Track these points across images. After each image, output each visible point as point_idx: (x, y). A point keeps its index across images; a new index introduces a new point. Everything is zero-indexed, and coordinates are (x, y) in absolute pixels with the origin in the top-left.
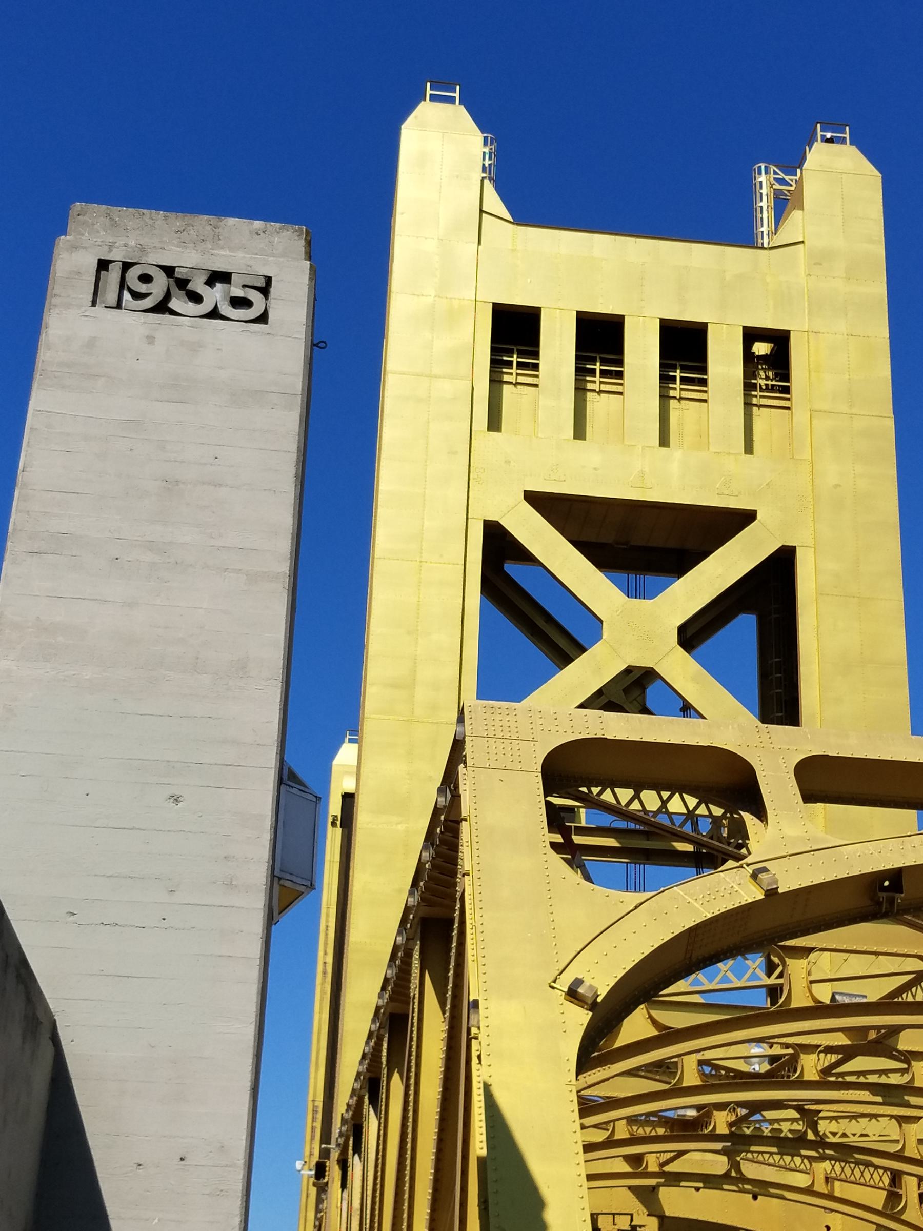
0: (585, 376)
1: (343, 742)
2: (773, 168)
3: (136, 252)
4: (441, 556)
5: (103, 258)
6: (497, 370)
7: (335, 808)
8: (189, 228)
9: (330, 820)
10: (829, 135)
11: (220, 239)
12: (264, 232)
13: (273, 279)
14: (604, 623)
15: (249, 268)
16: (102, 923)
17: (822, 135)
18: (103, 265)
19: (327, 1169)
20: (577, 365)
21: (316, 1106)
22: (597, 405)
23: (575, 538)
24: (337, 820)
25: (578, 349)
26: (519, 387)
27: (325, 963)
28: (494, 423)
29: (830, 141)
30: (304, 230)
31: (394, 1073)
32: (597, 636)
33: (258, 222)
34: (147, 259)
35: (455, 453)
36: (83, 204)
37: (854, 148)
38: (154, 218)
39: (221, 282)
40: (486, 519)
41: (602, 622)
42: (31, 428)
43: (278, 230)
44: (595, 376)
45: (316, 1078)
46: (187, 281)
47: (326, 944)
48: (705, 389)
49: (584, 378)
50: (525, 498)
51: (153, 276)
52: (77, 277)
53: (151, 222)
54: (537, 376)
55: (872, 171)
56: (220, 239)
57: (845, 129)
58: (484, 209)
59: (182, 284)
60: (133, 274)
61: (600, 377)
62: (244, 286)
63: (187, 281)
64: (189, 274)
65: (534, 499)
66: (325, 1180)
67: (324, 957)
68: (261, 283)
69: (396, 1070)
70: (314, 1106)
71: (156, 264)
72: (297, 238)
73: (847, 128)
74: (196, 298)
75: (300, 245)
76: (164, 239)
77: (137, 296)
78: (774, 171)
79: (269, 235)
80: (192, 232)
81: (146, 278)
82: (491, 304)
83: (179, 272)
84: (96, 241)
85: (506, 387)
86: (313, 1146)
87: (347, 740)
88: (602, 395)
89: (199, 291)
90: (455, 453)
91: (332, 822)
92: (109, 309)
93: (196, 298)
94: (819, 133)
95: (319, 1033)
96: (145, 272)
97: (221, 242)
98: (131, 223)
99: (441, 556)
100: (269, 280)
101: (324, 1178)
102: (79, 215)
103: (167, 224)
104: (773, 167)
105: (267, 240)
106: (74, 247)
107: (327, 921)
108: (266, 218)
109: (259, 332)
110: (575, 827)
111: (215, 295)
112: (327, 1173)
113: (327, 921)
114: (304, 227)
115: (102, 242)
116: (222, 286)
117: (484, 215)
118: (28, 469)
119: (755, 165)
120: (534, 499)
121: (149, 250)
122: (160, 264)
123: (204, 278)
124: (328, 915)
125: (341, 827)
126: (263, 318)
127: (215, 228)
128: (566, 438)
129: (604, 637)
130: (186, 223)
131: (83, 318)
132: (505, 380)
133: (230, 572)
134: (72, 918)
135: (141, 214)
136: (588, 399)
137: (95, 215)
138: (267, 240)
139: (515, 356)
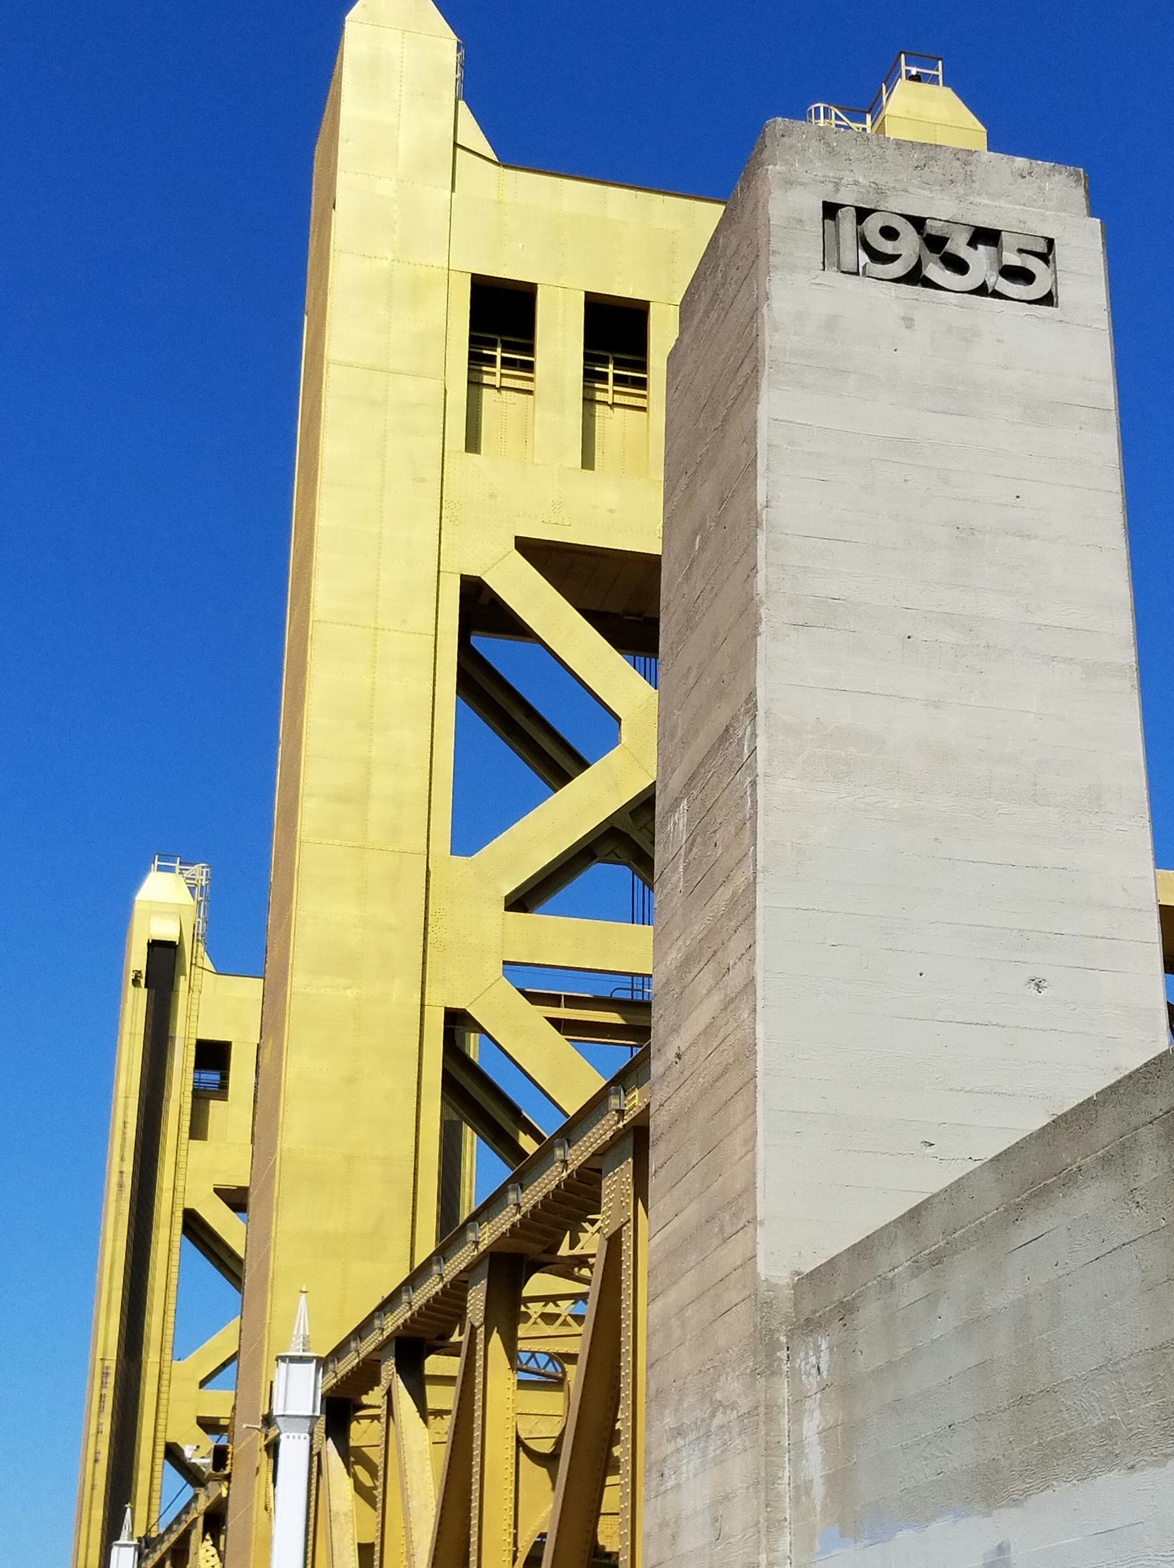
0: (594, 382)
1: (148, 870)
2: (834, 110)
3: (871, 194)
4: (404, 622)
5: (828, 200)
6: (477, 367)
7: (138, 959)
8: (930, 163)
9: (132, 976)
10: (914, 71)
11: (973, 181)
12: (1030, 174)
13: (1056, 241)
14: (622, 722)
15: (1022, 225)
16: (970, 1158)
17: (906, 70)
18: (830, 210)
19: (230, 1456)
20: (587, 367)
21: (107, 1367)
22: (609, 421)
23: (584, 607)
24: (141, 977)
25: (588, 344)
26: (504, 392)
27: (121, 1172)
28: (473, 443)
29: (917, 78)
30: (1082, 173)
31: (492, 1332)
32: (613, 740)
33: (1020, 159)
34: (887, 205)
35: (423, 480)
36: (787, 120)
37: (949, 91)
38: (884, 146)
39: (986, 244)
40: (464, 574)
41: (618, 720)
42: (768, 445)
43: (1048, 172)
44: (607, 384)
45: (106, 1329)
46: (943, 241)
47: (123, 1147)
48: (639, 402)
49: (591, 384)
50: (516, 548)
51: (899, 231)
52: (798, 226)
53: (878, 151)
54: (532, 380)
55: (974, 124)
56: (973, 181)
57: (937, 64)
58: (459, 142)
59: (935, 243)
60: (873, 225)
61: (614, 385)
62: (1021, 251)
63: (943, 241)
64: (946, 230)
65: (528, 548)
66: (227, 1472)
67: (120, 1164)
68: (1041, 248)
69: (496, 1329)
70: (103, 1367)
71: (900, 212)
72: (1074, 185)
73: (940, 63)
74: (958, 266)
75: (1078, 194)
76: (901, 177)
77: (878, 257)
78: (836, 114)
79: (1037, 178)
80: (936, 168)
81: (889, 233)
82: (470, 275)
83: (931, 226)
84: (816, 175)
85: (486, 392)
86: (101, 1421)
87: (154, 867)
88: (615, 409)
89: (962, 256)
90: (423, 480)
91: (133, 980)
92: (847, 275)
93: (958, 266)
94: (904, 68)
95: (112, 1267)
96: (886, 224)
97: (976, 185)
98: (853, 151)
99: (404, 622)
100: (1050, 243)
101: (225, 1469)
102: (783, 136)
103: (901, 155)
104: (835, 109)
105: (1035, 185)
106: (789, 183)
107: (125, 1115)
108: (1032, 155)
109: (1048, 318)
110: (565, 996)
111: (980, 260)
112: (229, 1462)
113: (125, 1115)
114: (1082, 170)
115: (824, 176)
116: (986, 249)
117: (458, 150)
118: (773, 504)
119: (812, 104)
120: (528, 548)
121: (887, 191)
122: (904, 213)
123: (965, 236)
124: (126, 1108)
125: (146, 987)
126: (1048, 299)
127: (966, 165)
128: (573, 466)
129: (622, 741)
130: (926, 155)
131: (814, 287)
132: (484, 382)
133: (1059, 662)
134: (929, 1150)
135: (866, 138)
136: (597, 414)
137: (804, 136)
138: (1035, 185)
139: (499, 350)
